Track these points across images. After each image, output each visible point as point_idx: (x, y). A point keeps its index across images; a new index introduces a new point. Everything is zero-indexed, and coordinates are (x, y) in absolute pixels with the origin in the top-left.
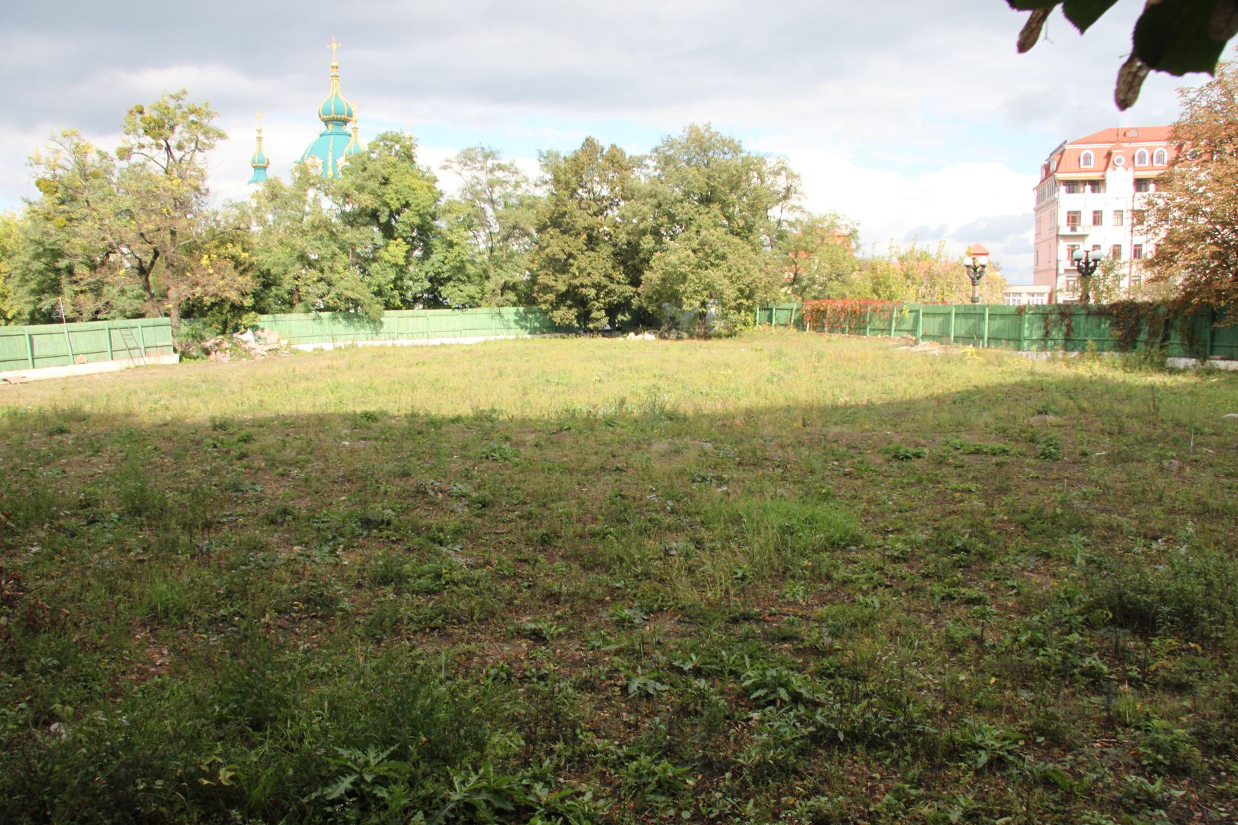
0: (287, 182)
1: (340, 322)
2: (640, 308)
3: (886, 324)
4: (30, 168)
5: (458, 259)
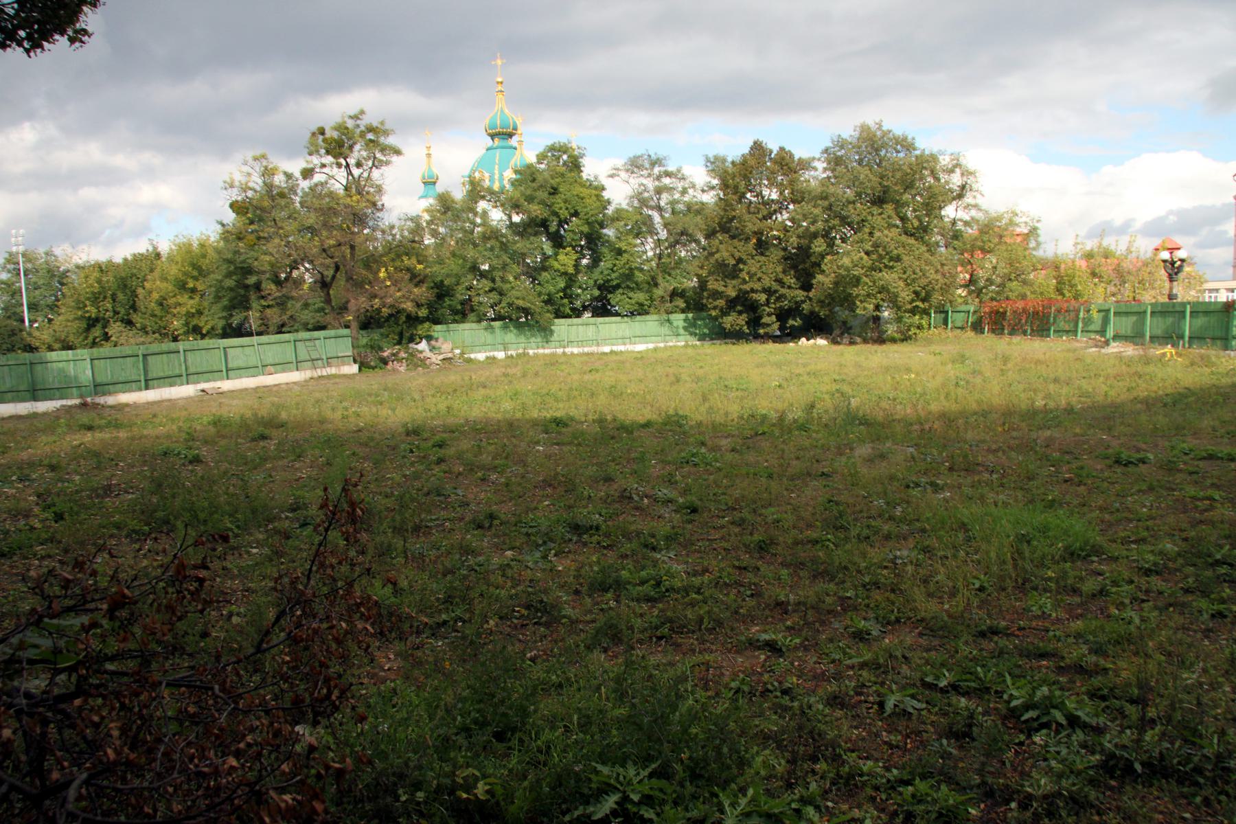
0: (459, 194)
1: (511, 331)
2: (812, 313)
3: (1072, 325)
4: (225, 192)
5: (627, 266)
